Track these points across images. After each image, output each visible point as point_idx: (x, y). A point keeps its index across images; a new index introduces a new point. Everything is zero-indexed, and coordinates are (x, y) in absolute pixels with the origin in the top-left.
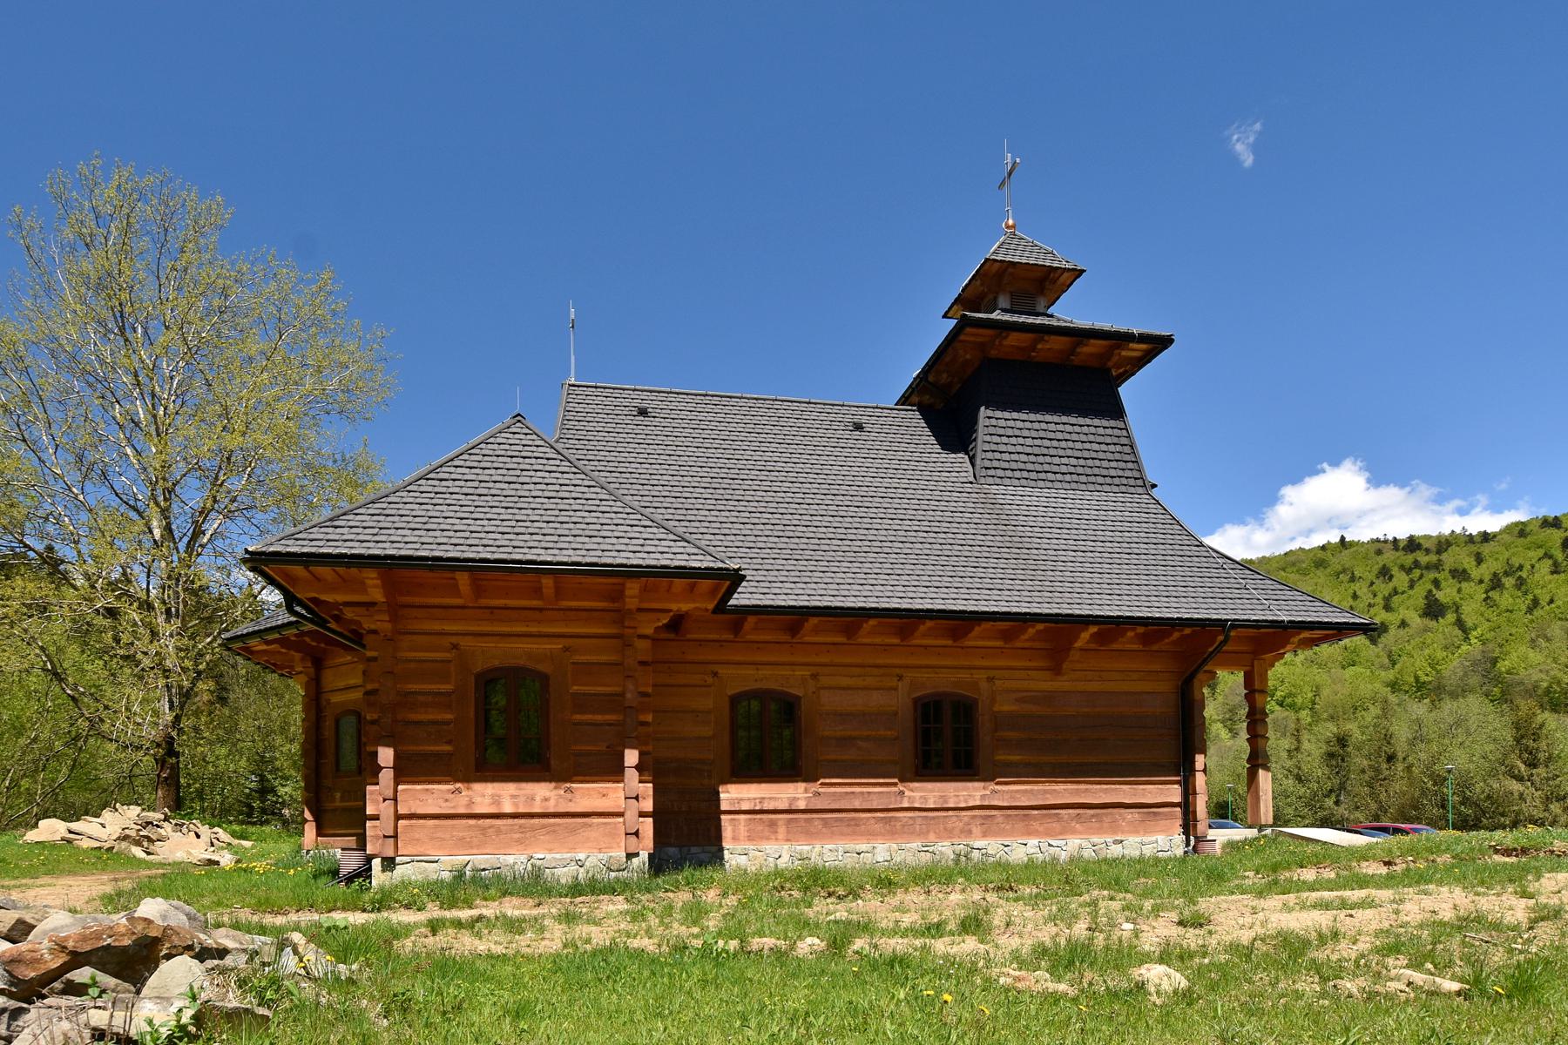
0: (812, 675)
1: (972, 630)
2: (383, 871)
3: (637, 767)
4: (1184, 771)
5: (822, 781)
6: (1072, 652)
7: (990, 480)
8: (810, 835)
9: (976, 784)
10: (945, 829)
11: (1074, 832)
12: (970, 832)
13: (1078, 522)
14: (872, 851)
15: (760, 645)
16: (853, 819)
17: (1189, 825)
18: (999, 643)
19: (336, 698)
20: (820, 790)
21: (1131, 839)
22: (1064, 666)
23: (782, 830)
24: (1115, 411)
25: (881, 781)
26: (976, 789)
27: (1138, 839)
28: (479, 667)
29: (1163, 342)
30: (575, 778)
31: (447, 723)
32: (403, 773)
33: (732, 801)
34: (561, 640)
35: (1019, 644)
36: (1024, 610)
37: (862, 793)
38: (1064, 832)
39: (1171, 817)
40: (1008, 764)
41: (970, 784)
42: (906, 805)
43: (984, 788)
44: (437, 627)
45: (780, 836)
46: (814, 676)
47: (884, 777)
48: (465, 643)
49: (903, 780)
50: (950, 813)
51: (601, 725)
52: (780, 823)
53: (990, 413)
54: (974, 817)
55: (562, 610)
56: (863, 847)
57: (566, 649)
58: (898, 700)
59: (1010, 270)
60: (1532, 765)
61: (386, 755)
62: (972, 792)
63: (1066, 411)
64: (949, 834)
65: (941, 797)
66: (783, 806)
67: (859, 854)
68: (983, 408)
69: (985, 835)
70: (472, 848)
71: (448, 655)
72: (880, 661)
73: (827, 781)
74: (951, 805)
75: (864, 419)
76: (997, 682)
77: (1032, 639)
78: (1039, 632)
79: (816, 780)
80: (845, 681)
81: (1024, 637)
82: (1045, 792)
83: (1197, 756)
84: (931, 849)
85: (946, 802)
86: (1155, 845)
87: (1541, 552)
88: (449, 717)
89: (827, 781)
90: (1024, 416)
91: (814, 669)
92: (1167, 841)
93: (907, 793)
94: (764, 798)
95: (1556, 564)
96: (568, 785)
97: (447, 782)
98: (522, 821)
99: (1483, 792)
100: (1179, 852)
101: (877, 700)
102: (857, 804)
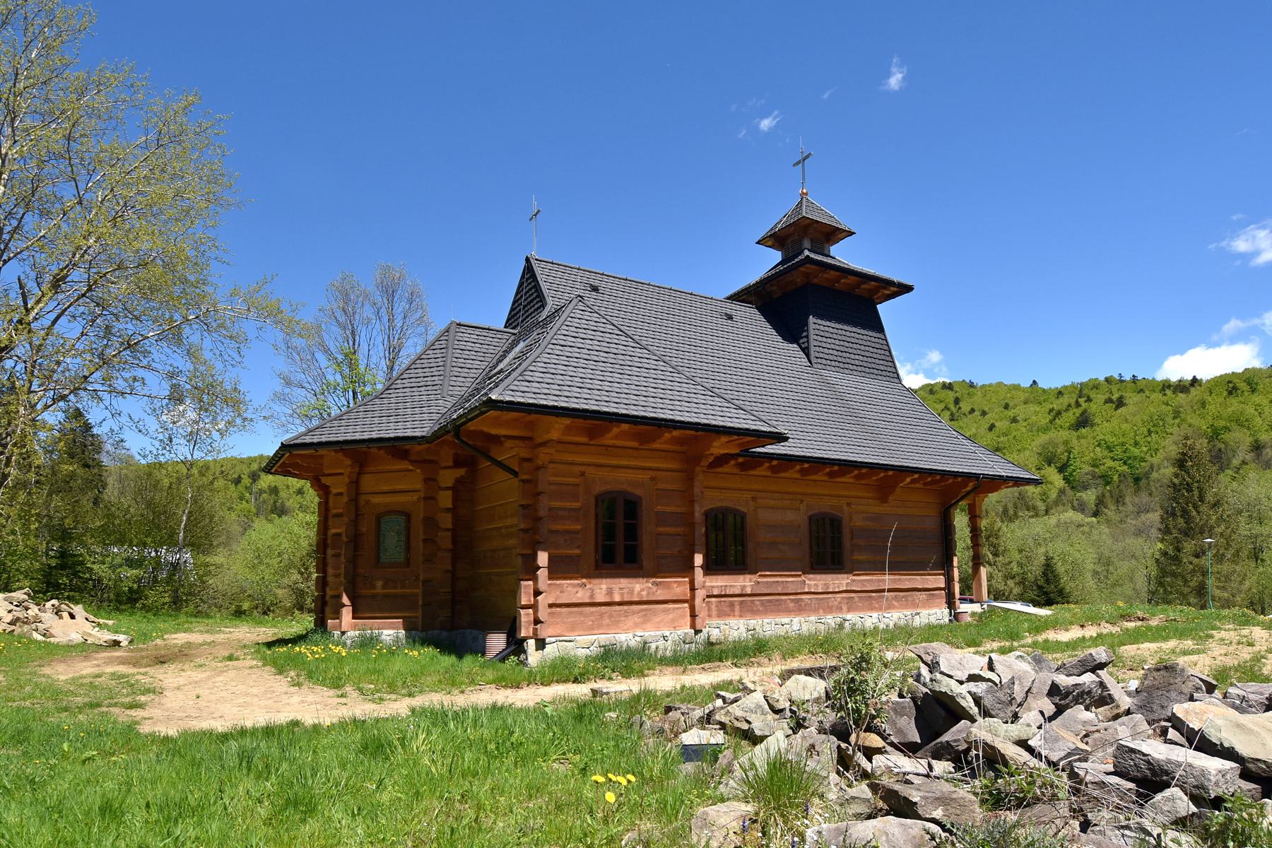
0: (752, 498)
1: (609, 430)
2: (537, 650)
3: (701, 567)
4: (945, 565)
6: (897, 489)
7: (820, 366)
8: (754, 612)
9: (843, 576)
10: (828, 606)
11: (894, 607)
12: (841, 609)
13: (593, 333)
14: (791, 623)
15: (722, 475)
16: (777, 600)
17: (951, 604)
18: (634, 444)
19: (376, 500)
20: (759, 580)
22: (890, 498)
23: (737, 608)
24: (876, 325)
25: (793, 573)
26: (843, 579)
27: (927, 612)
28: (598, 489)
29: (908, 289)
30: (659, 575)
31: (577, 532)
32: (555, 572)
34: (650, 472)
35: (656, 446)
36: (551, 403)
37: (782, 582)
38: (890, 607)
39: (939, 597)
41: (840, 576)
42: (806, 590)
44: (570, 458)
45: (737, 613)
46: (754, 499)
47: (794, 571)
48: (590, 471)
49: (804, 573)
50: (830, 596)
51: (674, 535)
52: (736, 604)
53: (815, 321)
54: (843, 598)
55: (603, 446)
56: (786, 620)
57: (652, 479)
58: (797, 516)
59: (815, 225)
60: (996, 555)
61: (543, 558)
62: (840, 581)
64: (829, 610)
65: (825, 584)
66: (738, 592)
68: (811, 317)
69: (849, 610)
70: (593, 629)
71: (578, 480)
72: (790, 490)
73: (763, 573)
75: (733, 313)
76: (853, 506)
77: (617, 437)
78: (673, 437)
79: (756, 573)
80: (772, 503)
81: (609, 435)
84: (822, 621)
85: (828, 588)
87: (942, 406)
88: (579, 527)
89: (763, 573)
90: (833, 325)
91: (754, 494)
92: (938, 614)
93: (807, 582)
94: (726, 586)
95: (952, 414)
96: (654, 580)
97: (576, 578)
98: (625, 607)
99: (177, 505)
100: (947, 620)
101: (790, 516)
102: (780, 590)
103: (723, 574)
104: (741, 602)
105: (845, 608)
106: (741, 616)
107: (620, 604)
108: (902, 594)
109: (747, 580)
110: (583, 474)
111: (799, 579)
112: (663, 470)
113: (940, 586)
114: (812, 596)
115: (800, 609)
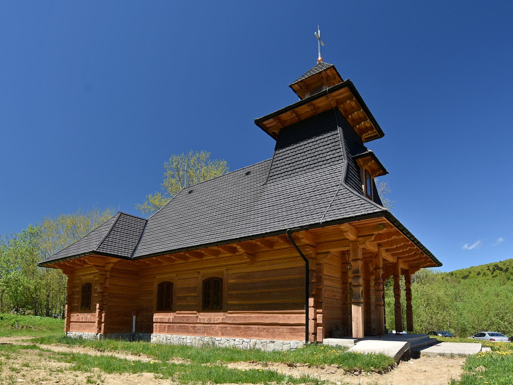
5: (228, 312)
12: (218, 333)
16: (184, 326)
21: (278, 341)
25: (188, 312)
26: (221, 316)
27: (281, 341)
33: (156, 318)
40: (232, 305)
41: (219, 314)
42: (198, 321)
43: (224, 315)
49: (199, 312)
50: (213, 325)
52: (166, 327)
54: (220, 327)
56: (184, 337)
62: (218, 317)
63: (310, 137)
66: (166, 321)
67: (183, 339)
74: (212, 322)
82: (245, 318)
83: (309, 299)
84: (202, 339)
85: (210, 321)
86: (289, 345)
93: (200, 317)
94: (162, 318)
103: (163, 312)
104: (168, 326)
105: (220, 333)
106: (167, 333)
107: (85, 322)
108: (264, 327)
109: (172, 315)
110: (80, 279)
111: (196, 315)
112: (239, 264)
113: (301, 322)
114: (203, 325)
115: (195, 331)
